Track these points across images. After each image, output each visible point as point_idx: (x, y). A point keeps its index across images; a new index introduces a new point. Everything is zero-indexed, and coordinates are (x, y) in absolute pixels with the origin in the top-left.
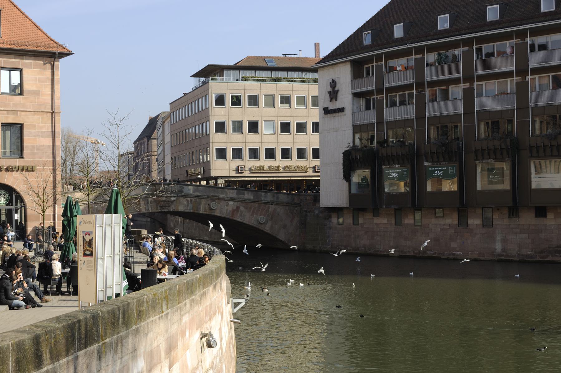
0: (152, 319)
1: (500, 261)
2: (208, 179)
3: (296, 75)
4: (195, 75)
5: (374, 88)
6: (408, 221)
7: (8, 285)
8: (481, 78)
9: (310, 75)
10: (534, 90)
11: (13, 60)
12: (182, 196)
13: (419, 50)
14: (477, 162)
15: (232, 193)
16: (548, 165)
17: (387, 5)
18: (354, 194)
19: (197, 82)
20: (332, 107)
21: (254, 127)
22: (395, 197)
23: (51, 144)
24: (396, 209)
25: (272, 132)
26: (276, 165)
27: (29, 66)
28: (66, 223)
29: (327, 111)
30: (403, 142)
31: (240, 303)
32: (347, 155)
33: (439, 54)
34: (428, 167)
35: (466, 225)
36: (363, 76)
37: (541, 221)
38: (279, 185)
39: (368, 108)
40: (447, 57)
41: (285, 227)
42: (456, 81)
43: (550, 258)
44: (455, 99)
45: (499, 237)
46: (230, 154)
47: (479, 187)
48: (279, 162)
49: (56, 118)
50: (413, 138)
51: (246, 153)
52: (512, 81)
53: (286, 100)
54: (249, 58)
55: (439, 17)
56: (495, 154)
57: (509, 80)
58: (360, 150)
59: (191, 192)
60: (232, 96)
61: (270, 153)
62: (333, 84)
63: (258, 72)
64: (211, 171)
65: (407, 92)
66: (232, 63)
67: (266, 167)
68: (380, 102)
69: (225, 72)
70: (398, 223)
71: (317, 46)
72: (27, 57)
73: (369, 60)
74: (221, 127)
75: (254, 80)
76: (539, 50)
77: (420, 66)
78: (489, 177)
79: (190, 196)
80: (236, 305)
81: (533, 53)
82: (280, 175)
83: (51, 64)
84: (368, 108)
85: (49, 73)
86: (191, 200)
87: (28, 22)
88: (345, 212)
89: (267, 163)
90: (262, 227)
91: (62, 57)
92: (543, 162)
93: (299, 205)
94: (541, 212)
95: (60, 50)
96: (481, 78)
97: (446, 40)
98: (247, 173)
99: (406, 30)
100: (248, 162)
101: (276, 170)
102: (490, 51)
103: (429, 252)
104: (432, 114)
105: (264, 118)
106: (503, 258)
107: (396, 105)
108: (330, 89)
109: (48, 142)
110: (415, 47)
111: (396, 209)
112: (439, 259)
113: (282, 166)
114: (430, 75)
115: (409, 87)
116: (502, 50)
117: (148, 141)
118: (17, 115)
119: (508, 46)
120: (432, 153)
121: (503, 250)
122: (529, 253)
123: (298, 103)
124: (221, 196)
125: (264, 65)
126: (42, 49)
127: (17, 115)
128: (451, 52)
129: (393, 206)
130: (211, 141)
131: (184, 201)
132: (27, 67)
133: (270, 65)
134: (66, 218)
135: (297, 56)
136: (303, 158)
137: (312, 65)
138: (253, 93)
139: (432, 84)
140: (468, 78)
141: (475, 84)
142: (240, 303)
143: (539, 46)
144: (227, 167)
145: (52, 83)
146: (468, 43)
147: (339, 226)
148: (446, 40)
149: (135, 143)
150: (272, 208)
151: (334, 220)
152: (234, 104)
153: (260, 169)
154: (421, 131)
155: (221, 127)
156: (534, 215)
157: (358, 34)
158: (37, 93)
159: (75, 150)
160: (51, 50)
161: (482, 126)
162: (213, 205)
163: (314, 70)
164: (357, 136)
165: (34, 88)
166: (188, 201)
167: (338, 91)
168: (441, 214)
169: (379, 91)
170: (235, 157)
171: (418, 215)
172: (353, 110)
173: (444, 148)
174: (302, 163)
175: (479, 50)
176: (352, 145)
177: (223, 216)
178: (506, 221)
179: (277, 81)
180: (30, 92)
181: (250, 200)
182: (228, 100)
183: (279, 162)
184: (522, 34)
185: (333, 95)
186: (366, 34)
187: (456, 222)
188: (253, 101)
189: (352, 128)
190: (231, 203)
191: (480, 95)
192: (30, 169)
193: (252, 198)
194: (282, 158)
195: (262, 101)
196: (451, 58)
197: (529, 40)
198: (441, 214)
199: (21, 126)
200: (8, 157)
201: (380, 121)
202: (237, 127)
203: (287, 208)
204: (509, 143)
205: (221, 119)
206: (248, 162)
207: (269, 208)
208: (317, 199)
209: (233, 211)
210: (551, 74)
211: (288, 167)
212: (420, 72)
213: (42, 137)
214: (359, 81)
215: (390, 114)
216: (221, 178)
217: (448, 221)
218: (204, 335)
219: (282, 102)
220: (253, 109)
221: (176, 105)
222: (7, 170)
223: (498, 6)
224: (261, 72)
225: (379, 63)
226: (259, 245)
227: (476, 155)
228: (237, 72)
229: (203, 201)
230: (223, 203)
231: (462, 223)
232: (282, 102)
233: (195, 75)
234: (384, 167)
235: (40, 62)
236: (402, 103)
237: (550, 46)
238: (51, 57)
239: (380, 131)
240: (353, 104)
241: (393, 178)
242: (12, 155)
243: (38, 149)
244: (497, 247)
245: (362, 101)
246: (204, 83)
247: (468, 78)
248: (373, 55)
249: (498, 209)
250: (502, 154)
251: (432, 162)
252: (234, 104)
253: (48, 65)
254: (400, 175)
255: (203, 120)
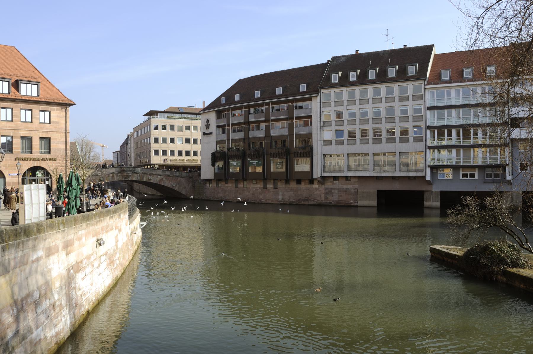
0: (49, 233)
1: (281, 204)
2: (151, 165)
3: (193, 116)
4: (145, 115)
5: (226, 123)
6: (241, 185)
7: (16, 216)
8: (273, 120)
9: (198, 116)
10: (296, 127)
11: (46, 107)
12: (135, 173)
13: (246, 107)
14: (271, 159)
15: (160, 172)
16: (302, 161)
17: (233, 85)
18: (216, 173)
19: (147, 117)
20: (207, 132)
21: (172, 141)
22: (234, 174)
23: (65, 148)
24: (235, 180)
25: (181, 143)
26: (183, 159)
27: (54, 110)
28: (59, 186)
29: (204, 134)
30: (239, 149)
31: (144, 224)
32: (213, 154)
33: (255, 109)
34: (249, 161)
35: (267, 188)
36: (221, 118)
37: (299, 186)
38: (185, 168)
39: (223, 133)
40: (258, 110)
41: (185, 188)
42: (262, 122)
43: (303, 203)
44: (262, 130)
45: (280, 193)
46: (161, 153)
47: (272, 170)
48: (184, 157)
49: (67, 135)
50: (243, 148)
51: (169, 153)
52: (287, 122)
53: (188, 128)
54: (171, 107)
55: (255, 92)
56: (279, 155)
57: (286, 121)
58: (220, 152)
59: (140, 171)
60: (162, 126)
61: (180, 153)
62: (208, 121)
63: (175, 114)
64: (152, 161)
65: (241, 126)
66: (163, 110)
67: (178, 159)
68: (228, 130)
69: (159, 114)
70: (236, 187)
71: (204, 103)
72: (53, 106)
73: (224, 110)
74: (156, 140)
75: (173, 118)
76: (299, 108)
77: (247, 114)
78: (276, 166)
79: (139, 173)
80: (142, 225)
81: (296, 110)
82: (192, 163)
83: (65, 109)
84: (223, 133)
85: (64, 113)
86: (139, 175)
87: (54, 88)
88: (213, 181)
89: (179, 158)
90: (174, 188)
91: (71, 106)
92: (300, 159)
93: (192, 177)
94: (299, 182)
95: (70, 102)
96: (273, 120)
97: (258, 102)
98: (169, 162)
99: (261, 94)
100: (169, 157)
101: (183, 161)
102: (278, 108)
103: (250, 200)
104: (252, 136)
105: (177, 136)
106: (282, 202)
107: (236, 132)
108: (206, 124)
109: (63, 147)
110: (244, 105)
111: (235, 180)
112: (254, 203)
113: (186, 159)
114: (251, 118)
115: (241, 124)
116: (283, 108)
117: (127, 146)
118: (47, 133)
119: (285, 106)
120: (282, 153)
121: (282, 199)
122: (294, 200)
123: (194, 130)
124: (154, 173)
125: (178, 111)
126: (61, 102)
127: (47, 133)
128: (260, 109)
129: (234, 179)
130: (151, 147)
131: (136, 175)
132: (53, 110)
133: (181, 111)
134: (59, 184)
135: (194, 107)
136: (196, 155)
137: (198, 112)
138: (172, 124)
139: (252, 122)
140: (268, 120)
141: (294, 121)
142: (144, 224)
143: (299, 107)
144: (159, 159)
145: (65, 118)
146: (267, 104)
147: (210, 188)
148: (258, 102)
149: (120, 147)
150: (179, 179)
151: (208, 185)
152: (163, 129)
153: (175, 161)
154: (246, 144)
155: (156, 140)
156: (296, 183)
157: (219, 99)
158: (58, 123)
159: (90, 150)
160: (65, 102)
161: (298, 140)
162: (150, 177)
163: (199, 114)
164: (218, 146)
165: (56, 120)
166: (138, 175)
167: (210, 124)
168: (255, 183)
169: (228, 125)
170: (163, 154)
171: (245, 183)
172: (216, 133)
173: (256, 152)
174: (195, 158)
175: (273, 108)
176: (215, 150)
177: (155, 182)
178: (284, 186)
179: (184, 119)
180: (55, 123)
181: (168, 175)
182: (160, 128)
183: (184, 157)
184: (291, 101)
185: (208, 126)
186: (223, 98)
187: (262, 186)
188: (172, 128)
189: (216, 142)
190: (159, 176)
191: (273, 128)
192: (54, 160)
193: (169, 174)
194: (186, 155)
195: (176, 128)
196: (260, 111)
197: (295, 104)
198: (255, 183)
199: (49, 139)
200: (43, 154)
201: (228, 139)
202: (165, 140)
203: (186, 179)
204: (285, 151)
205: (156, 136)
206: (169, 157)
207: (177, 179)
208: (200, 175)
209: (160, 180)
210: (304, 120)
211: (189, 160)
212: (247, 117)
213: (60, 144)
214: (219, 120)
215: (233, 136)
216: (157, 164)
217: (259, 186)
218: (98, 240)
219: (186, 129)
220: (172, 132)
221: (136, 129)
222: (42, 160)
223: (305, 84)
224: (176, 114)
225: (228, 112)
226: (192, 197)
227: (271, 156)
228: (165, 114)
229: (145, 176)
230: (155, 176)
231: (265, 187)
232: (186, 129)
233: (145, 115)
234: (230, 160)
235: (59, 108)
236: (239, 131)
237: (304, 107)
238: (65, 105)
239: (228, 144)
240: (217, 131)
241: (234, 165)
242: (45, 153)
243: (58, 150)
244: (280, 198)
245: (221, 130)
246: (149, 119)
247: (268, 120)
248: (225, 108)
249: (281, 181)
250: (306, 154)
251: (251, 158)
252: (163, 129)
253: (64, 110)
254: (237, 164)
255: (148, 137)
